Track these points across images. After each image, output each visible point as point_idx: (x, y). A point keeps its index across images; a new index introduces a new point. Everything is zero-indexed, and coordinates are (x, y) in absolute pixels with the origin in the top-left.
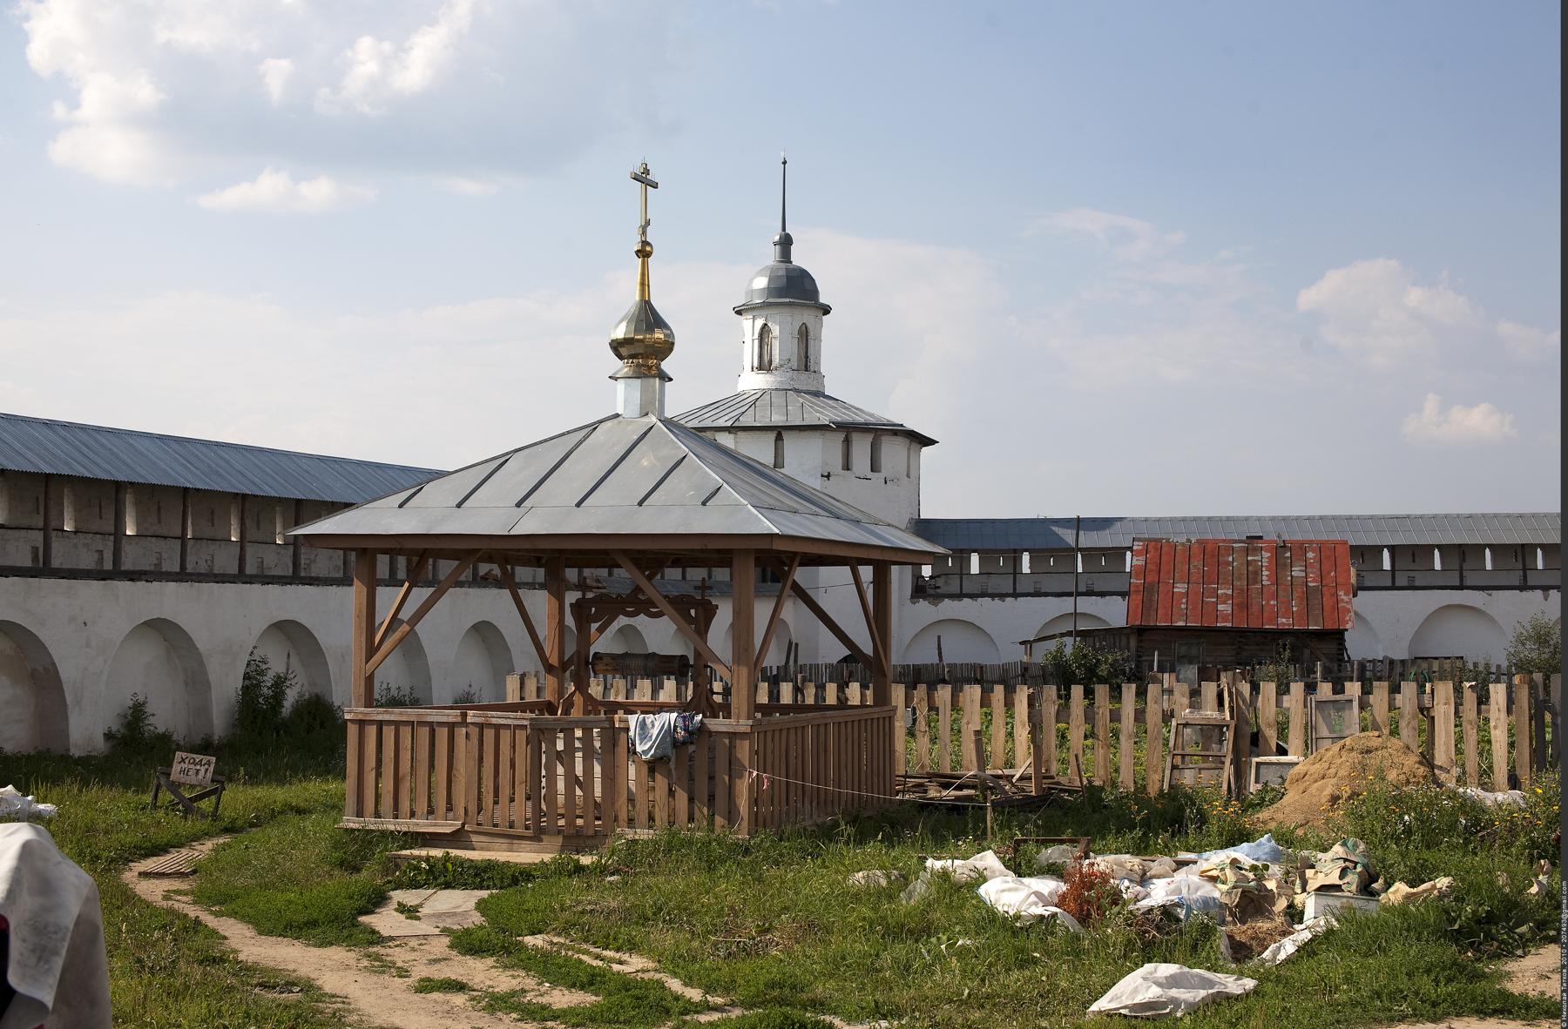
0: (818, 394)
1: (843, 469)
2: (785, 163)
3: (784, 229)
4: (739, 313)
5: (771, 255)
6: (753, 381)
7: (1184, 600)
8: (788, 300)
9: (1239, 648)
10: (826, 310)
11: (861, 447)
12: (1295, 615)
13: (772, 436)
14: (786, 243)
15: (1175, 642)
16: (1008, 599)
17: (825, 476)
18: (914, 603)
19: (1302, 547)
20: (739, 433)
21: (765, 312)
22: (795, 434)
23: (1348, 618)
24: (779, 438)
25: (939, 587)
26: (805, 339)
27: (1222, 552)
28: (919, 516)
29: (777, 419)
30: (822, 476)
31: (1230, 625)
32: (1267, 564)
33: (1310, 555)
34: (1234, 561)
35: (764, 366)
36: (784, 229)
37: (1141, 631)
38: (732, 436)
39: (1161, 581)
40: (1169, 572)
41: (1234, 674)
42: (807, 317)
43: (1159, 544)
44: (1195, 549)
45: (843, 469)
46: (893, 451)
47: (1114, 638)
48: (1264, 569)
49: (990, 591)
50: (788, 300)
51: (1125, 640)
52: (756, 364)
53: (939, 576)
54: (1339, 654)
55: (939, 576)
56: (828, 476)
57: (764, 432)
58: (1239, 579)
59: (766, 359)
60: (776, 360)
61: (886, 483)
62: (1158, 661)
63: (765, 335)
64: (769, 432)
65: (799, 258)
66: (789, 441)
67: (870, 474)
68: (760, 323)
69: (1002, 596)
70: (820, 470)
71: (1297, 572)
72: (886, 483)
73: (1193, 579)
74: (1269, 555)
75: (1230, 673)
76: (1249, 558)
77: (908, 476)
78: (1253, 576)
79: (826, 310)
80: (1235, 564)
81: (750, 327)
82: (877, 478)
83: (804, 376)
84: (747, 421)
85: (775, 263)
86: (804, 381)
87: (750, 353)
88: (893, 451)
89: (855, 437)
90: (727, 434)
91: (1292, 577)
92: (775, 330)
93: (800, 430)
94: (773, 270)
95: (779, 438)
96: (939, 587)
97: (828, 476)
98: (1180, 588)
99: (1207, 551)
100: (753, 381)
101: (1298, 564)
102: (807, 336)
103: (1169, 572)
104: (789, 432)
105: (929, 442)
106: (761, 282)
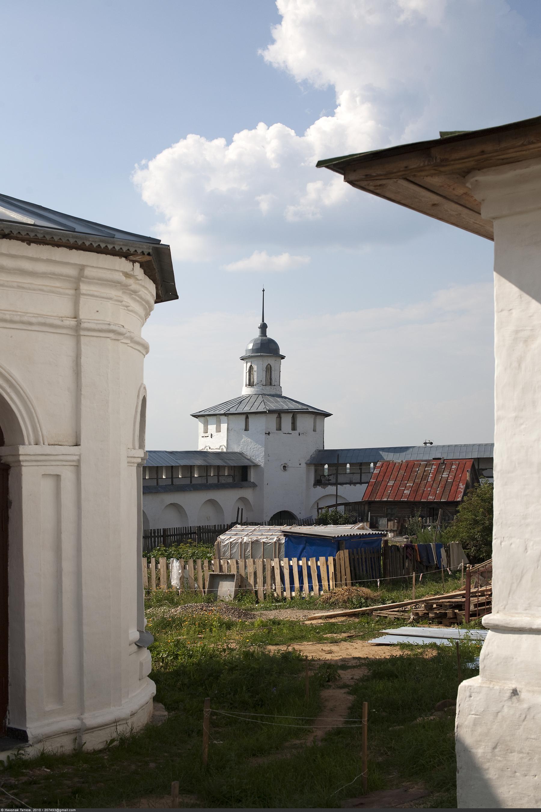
0: (280, 396)
1: (277, 430)
2: (264, 291)
3: (263, 321)
4: (242, 359)
5: (257, 333)
6: (246, 391)
7: (390, 489)
8: (259, 354)
9: (413, 509)
10: (283, 357)
11: (287, 421)
12: (437, 495)
13: (244, 417)
14: (264, 327)
15: (385, 508)
16: (357, 485)
17: (268, 434)
18: (315, 488)
19: (451, 462)
20: (229, 416)
21: (250, 360)
22: (253, 416)
23: (459, 496)
24: (247, 418)
25: (330, 480)
26: (270, 371)
27: (415, 466)
28: (324, 448)
29: (247, 409)
30: (266, 434)
31: (406, 500)
32: (433, 471)
33: (454, 467)
34: (420, 471)
35: (250, 384)
36: (263, 321)
37: (370, 503)
38: (226, 417)
39: (384, 480)
40: (388, 476)
41: (394, 523)
42: (271, 361)
43: (389, 463)
44: (404, 467)
45: (277, 430)
46: (304, 422)
47: (358, 506)
48: (431, 474)
49: (354, 481)
50: (259, 354)
51: (363, 507)
52: (247, 384)
53: (331, 475)
54: (265, 522)
55: (331, 475)
56: (269, 434)
57: (241, 415)
58: (418, 479)
59: (252, 380)
60: (255, 381)
61: (299, 435)
62: (370, 516)
63: (252, 370)
64: (242, 415)
65: (270, 334)
66: (251, 419)
67: (291, 432)
68: (249, 364)
69: (355, 484)
70: (265, 431)
71: (445, 475)
72: (299, 435)
73: (398, 479)
74: (435, 467)
75: (392, 522)
76: (426, 469)
77: (314, 430)
78: (424, 477)
79: (283, 357)
80: (419, 472)
81: (245, 366)
82: (296, 432)
83: (268, 388)
84: (233, 411)
85: (258, 337)
86: (269, 390)
87: (245, 379)
88: (304, 422)
89: (283, 415)
90: (224, 416)
91: (442, 476)
92: (255, 368)
93: (256, 414)
94: (255, 340)
95: (247, 418)
96: (330, 480)
97: (269, 434)
98: (391, 483)
99: (408, 466)
100: (246, 391)
101: (446, 471)
102: (271, 369)
103: (388, 476)
104: (251, 415)
105: (328, 415)
106: (251, 346)
